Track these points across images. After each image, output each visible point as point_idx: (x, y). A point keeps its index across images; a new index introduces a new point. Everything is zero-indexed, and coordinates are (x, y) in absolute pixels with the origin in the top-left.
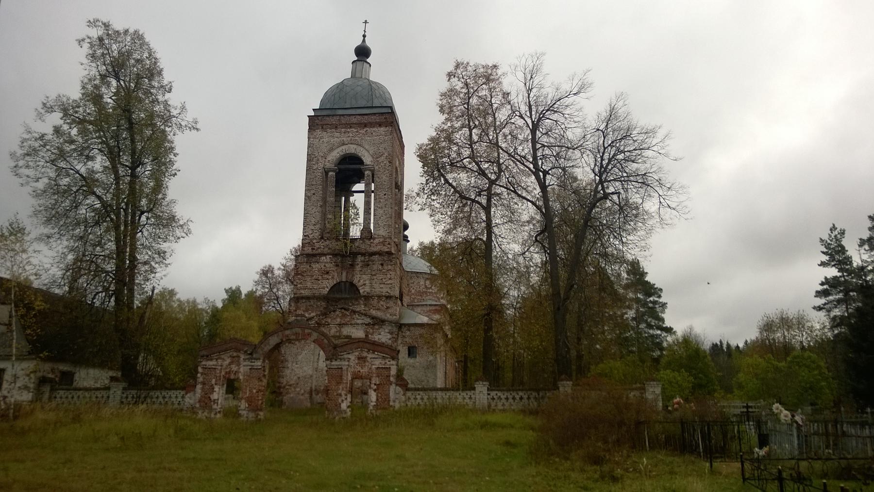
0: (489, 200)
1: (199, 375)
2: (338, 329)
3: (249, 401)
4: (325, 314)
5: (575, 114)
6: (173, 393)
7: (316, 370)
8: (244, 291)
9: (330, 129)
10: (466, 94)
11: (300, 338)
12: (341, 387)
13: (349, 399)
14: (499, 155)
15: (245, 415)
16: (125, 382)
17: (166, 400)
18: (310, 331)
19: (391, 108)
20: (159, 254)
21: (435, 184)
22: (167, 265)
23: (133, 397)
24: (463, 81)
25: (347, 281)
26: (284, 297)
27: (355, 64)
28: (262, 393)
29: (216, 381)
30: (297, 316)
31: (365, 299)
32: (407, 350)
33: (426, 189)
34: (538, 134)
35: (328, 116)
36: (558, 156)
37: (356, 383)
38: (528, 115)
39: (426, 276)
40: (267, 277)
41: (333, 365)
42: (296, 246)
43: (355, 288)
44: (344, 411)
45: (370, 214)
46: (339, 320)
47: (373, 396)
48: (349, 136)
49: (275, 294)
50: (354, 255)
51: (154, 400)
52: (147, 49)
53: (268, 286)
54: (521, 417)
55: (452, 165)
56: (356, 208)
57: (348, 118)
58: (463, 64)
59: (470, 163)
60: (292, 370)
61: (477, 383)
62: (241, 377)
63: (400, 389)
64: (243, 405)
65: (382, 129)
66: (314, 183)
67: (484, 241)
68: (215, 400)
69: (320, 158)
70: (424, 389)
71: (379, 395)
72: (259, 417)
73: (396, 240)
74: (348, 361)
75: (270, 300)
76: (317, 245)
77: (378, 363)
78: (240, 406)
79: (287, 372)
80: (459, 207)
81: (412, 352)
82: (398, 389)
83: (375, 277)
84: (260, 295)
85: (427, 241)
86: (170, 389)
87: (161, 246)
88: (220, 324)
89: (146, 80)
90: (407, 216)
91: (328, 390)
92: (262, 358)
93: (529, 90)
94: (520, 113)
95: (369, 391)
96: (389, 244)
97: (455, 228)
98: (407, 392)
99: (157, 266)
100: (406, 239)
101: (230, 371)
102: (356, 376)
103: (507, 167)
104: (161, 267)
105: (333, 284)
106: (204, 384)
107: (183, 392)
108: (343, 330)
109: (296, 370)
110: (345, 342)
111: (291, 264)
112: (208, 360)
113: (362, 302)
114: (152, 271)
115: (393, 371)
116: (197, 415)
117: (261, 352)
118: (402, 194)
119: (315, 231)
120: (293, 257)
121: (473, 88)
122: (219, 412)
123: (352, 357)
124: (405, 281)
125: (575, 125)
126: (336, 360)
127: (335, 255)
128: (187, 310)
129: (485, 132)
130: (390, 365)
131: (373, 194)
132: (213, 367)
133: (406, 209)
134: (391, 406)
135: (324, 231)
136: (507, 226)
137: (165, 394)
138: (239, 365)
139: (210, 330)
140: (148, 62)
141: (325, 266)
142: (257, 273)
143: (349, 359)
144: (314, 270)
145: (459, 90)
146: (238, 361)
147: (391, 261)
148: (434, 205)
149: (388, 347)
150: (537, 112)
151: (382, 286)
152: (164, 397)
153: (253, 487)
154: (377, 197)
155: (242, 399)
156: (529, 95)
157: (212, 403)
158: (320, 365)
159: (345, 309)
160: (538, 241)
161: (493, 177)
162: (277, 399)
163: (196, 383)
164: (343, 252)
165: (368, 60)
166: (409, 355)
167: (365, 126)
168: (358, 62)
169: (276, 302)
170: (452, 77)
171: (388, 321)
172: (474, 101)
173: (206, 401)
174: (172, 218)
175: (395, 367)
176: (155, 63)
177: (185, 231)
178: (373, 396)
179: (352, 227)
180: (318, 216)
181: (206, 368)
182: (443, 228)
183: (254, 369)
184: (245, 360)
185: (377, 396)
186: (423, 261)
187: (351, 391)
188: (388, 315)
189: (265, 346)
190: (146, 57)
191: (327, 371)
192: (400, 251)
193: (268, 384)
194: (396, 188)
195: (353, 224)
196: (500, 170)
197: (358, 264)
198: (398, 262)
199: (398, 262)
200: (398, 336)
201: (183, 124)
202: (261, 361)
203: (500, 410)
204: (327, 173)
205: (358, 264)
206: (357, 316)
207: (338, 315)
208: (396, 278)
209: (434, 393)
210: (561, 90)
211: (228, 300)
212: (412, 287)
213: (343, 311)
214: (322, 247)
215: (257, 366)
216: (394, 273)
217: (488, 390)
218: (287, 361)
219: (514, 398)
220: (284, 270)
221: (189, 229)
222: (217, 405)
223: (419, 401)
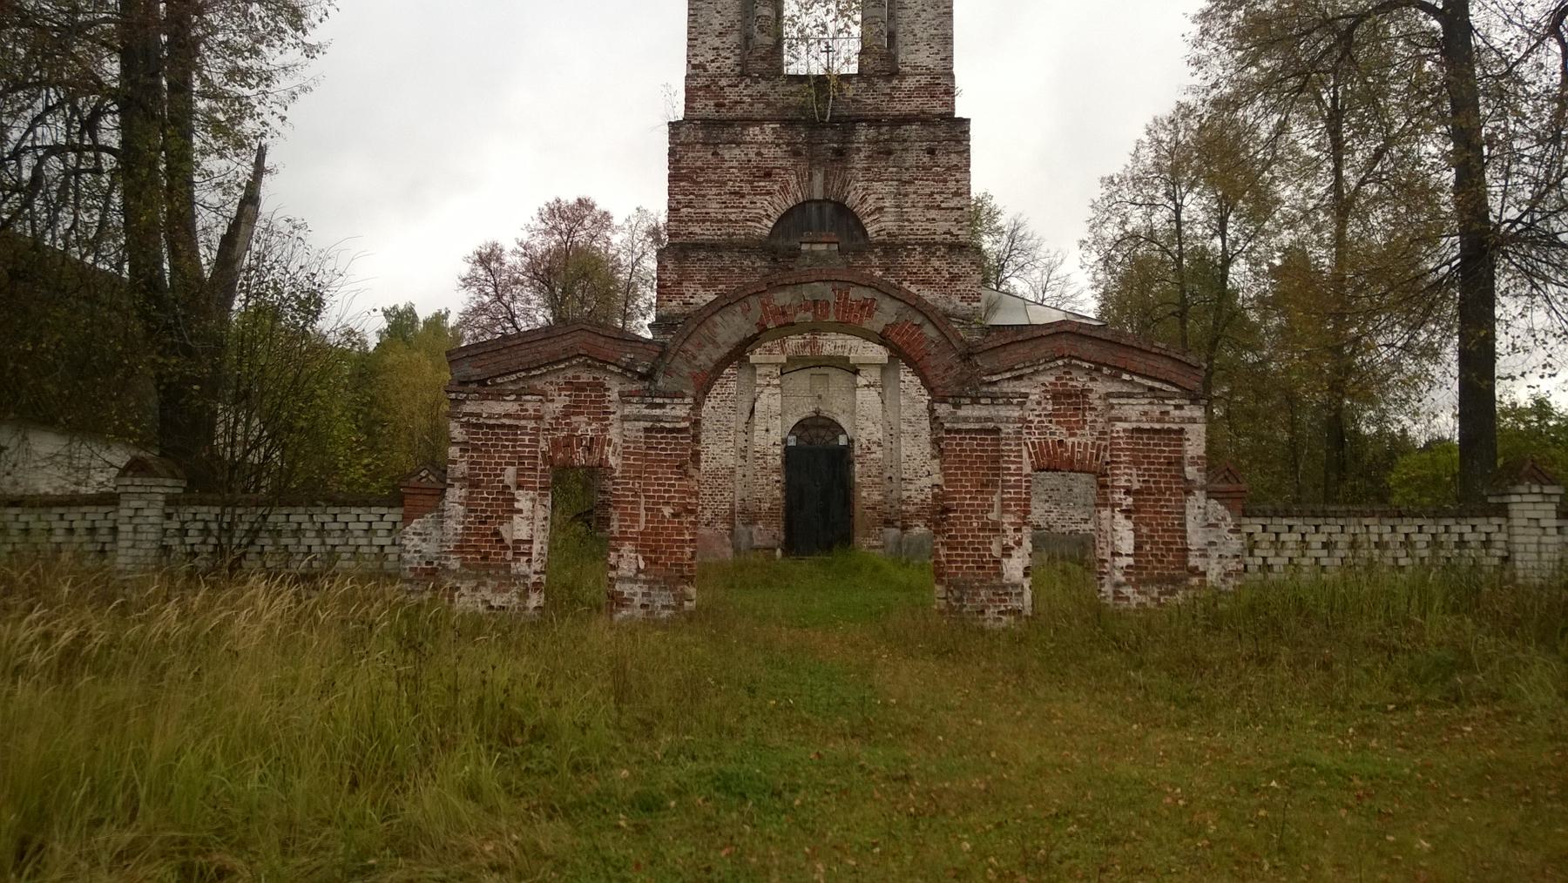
6: (356, 519)
15: (638, 600)
18: (867, 294)
22: (310, 51)
23: (206, 531)
25: (825, 200)
28: (692, 519)
41: (966, 419)
43: (851, 222)
44: (1015, 586)
50: (847, 124)
61: (1521, 489)
62: (612, 461)
71: (1145, 530)
74: (1021, 404)
76: (731, 95)
77: (1135, 412)
82: (1217, 508)
83: (911, 189)
91: (946, 510)
101: (570, 437)
105: (785, 207)
106: (473, 483)
107: (393, 515)
108: (821, 339)
113: (876, 261)
117: (686, 370)
122: (537, 586)
126: (975, 401)
127: (788, 123)
132: (507, 421)
134: (1194, 571)
137: (327, 519)
138: (602, 415)
141: (759, 154)
142: (467, 259)
143: (1026, 396)
144: (727, 164)
151: (933, 214)
152: (321, 532)
175: (1201, 428)
181: (479, 426)
183: (662, 429)
184: (625, 398)
188: (956, 299)
189: (700, 346)
205: (859, 150)
215: (677, 419)
222: (529, 561)
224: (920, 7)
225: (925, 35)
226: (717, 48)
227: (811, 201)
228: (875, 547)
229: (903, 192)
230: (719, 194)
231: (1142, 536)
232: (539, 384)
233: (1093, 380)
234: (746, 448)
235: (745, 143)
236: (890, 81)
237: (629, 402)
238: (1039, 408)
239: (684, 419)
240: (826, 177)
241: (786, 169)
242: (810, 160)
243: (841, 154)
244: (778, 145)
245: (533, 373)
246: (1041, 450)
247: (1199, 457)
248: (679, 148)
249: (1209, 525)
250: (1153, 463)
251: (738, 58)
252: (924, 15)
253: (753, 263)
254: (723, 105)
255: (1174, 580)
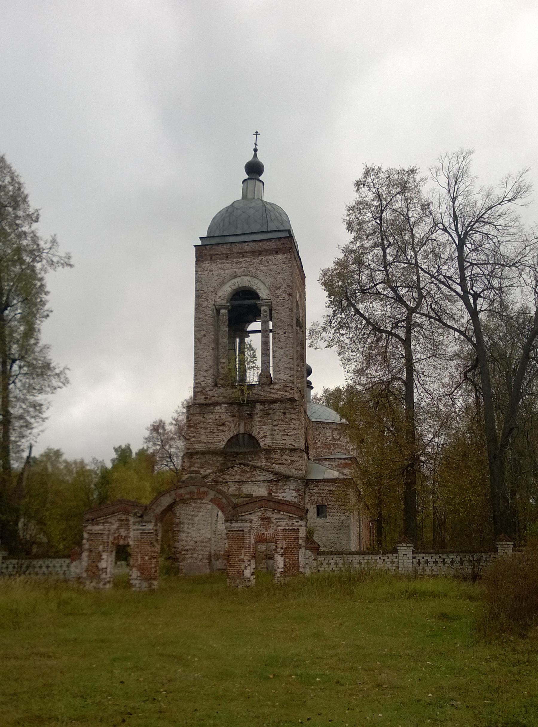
0: (409, 332)
1: (84, 541)
2: (238, 487)
3: (142, 569)
4: (222, 471)
5: (510, 224)
6: (57, 562)
7: (215, 532)
8: (135, 450)
9: (220, 259)
10: (377, 207)
11: (195, 497)
12: (243, 551)
13: (253, 566)
14: (418, 277)
15: (137, 585)
16: (4, 550)
17: (50, 569)
18: (205, 489)
19: (289, 231)
20: (34, 406)
21: (343, 316)
22: (44, 420)
23: (14, 567)
24: (374, 191)
25: (245, 433)
26: (177, 454)
27: (245, 183)
28: (155, 560)
29: (104, 547)
30: (191, 472)
31: (267, 453)
32: (315, 509)
33: (333, 322)
34: (466, 250)
35: (218, 244)
36: (492, 274)
37: (259, 547)
38: (453, 228)
39: (334, 426)
40: (158, 433)
41: (234, 527)
42: (188, 397)
43: (255, 441)
45: (269, 356)
46: (238, 477)
47: (280, 562)
48: (241, 267)
49: (168, 451)
51: (37, 570)
52: (9, 172)
53: (159, 443)
54: (455, 583)
55: (363, 291)
56: (252, 349)
57: (240, 245)
58: (373, 170)
59: (384, 289)
60: (188, 533)
61: (401, 545)
62: (131, 543)
63: (310, 553)
64: (135, 573)
65: (279, 256)
66: (205, 323)
67: (403, 381)
68: (103, 568)
69: (210, 294)
70: (340, 553)
71: (287, 560)
72: (153, 587)
73: (299, 385)
74: (251, 522)
75: (162, 458)
76: (210, 394)
77: (284, 524)
78: (131, 575)
79: (183, 536)
80: (372, 342)
81: (321, 511)
83: (276, 428)
84: (151, 453)
85: (332, 387)
86: (54, 558)
87: (37, 398)
88: (110, 486)
89: (10, 209)
90: (310, 361)
92: (154, 521)
93: (454, 199)
94: (444, 226)
95: (276, 555)
96: (291, 389)
97: (368, 367)
98: (319, 556)
99: (32, 420)
100: (309, 386)
101: (118, 536)
102: (260, 540)
103: (429, 293)
104: (38, 422)
106: (90, 551)
107: (68, 561)
109: (192, 533)
110: (246, 501)
111: (183, 418)
112: (93, 525)
113: (263, 457)
114: (28, 426)
115: (302, 533)
116: (84, 586)
117: (152, 514)
118: (304, 332)
119: (207, 378)
120: (185, 410)
121: (386, 200)
122: (109, 582)
123: (255, 518)
124: (310, 431)
125: (510, 238)
126: (237, 521)
127: (231, 404)
128: (75, 471)
129: (402, 250)
130: (298, 526)
131: (271, 334)
132: (100, 532)
133: (310, 346)
134: (301, 573)
135: (218, 377)
136: (431, 361)
137: (49, 562)
138: (128, 529)
139: (100, 493)
140: (11, 188)
141: (220, 417)
142: (147, 429)
143: (252, 520)
144: (208, 421)
145: (369, 202)
146: (127, 525)
147: (295, 409)
148: (342, 341)
149: (294, 505)
150: (463, 225)
151: (285, 437)
152: (48, 567)
153: (141, 679)
154: (276, 336)
155: (133, 566)
156: (454, 203)
157: (100, 572)
158: (218, 527)
159: (244, 465)
160: (468, 379)
161: (412, 305)
162: (173, 565)
163: (81, 550)
164: (239, 400)
165: (261, 178)
166: (318, 514)
167: (260, 254)
168: (249, 181)
169: (169, 460)
170: (362, 186)
171: (292, 477)
172: (387, 215)
173: (94, 570)
174: (47, 366)
176: (19, 189)
177: (62, 380)
178: (280, 562)
179: (248, 371)
180: (210, 361)
181: (92, 533)
182: (354, 367)
183: (145, 533)
184: (134, 523)
185: (285, 562)
186: (329, 410)
187: (254, 557)
188: (293, 470)
189: (157, 506)
190: (9, 182)
191: (227, 534)
192: (303, 398)
193: (162, 549)
194: (297, 326)
195: (249, 368)
196: (421, 296)
197: (257, 414)
198: (302, 410)
199: (302, 410)
200: (305, 494)
201: (55, 259)
202: (153, 524)
203: (429, 576)
204: (218, 311)
205: (257, 414)
206: (258, 472)
207: (236, 472)
208: (300, 428)
209: (350, 557)
210: (491, 197)
211: (117, 459)
212: (317, 439)
213: (242, 466)
214: (216, 395)
215: (149, 529)
216: (298, 422)
217: (413, 553)
218: (182, 523)
219: (444, 562)
220: (176, 425)
221: (66, 379)
223: (333, 566)
224: (281, 357)
225: (283, 368)
226: (205, 376)
227: (240, 434)
228: (263, 568)
229: (274, 429)
230: (205, 433)
231: (286, 562)
232: (110, 520)
233: (273, 514)
234: (215, 531)
235: (214, 413)
236: (270, 386)
237: (135, 525)
238: (257, 523)
239: (151, 529)
240: (245, 424)
241: (229, 422)
242: (239, 418)
243: (251, 415)
244: (227, 413)
245: (108, 517)
246: (257, 536)
247: (303, 537)
248: (190, 416)
249: (306, 558)
250: (290, 539)
251: (212, 380)
252: (282, 360)
253: (217, 459)
254: (207, 398)
255: (295, 575)
